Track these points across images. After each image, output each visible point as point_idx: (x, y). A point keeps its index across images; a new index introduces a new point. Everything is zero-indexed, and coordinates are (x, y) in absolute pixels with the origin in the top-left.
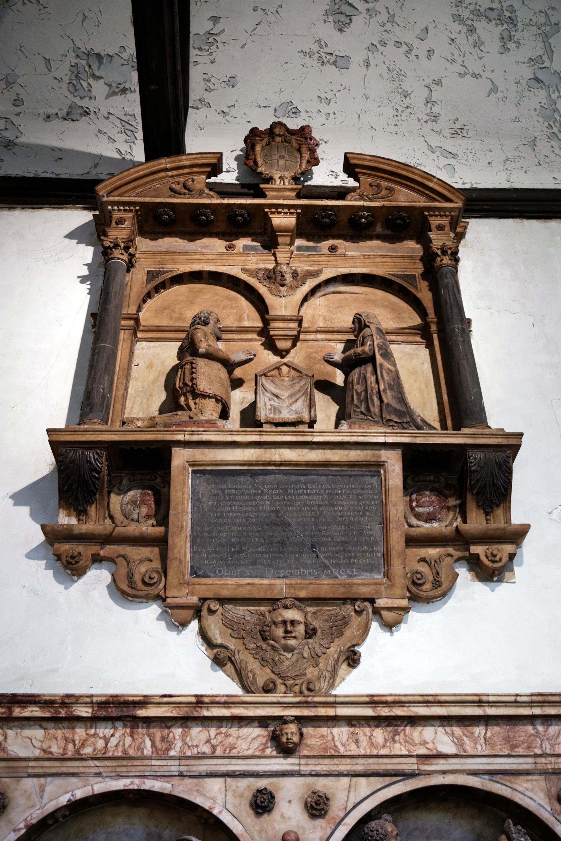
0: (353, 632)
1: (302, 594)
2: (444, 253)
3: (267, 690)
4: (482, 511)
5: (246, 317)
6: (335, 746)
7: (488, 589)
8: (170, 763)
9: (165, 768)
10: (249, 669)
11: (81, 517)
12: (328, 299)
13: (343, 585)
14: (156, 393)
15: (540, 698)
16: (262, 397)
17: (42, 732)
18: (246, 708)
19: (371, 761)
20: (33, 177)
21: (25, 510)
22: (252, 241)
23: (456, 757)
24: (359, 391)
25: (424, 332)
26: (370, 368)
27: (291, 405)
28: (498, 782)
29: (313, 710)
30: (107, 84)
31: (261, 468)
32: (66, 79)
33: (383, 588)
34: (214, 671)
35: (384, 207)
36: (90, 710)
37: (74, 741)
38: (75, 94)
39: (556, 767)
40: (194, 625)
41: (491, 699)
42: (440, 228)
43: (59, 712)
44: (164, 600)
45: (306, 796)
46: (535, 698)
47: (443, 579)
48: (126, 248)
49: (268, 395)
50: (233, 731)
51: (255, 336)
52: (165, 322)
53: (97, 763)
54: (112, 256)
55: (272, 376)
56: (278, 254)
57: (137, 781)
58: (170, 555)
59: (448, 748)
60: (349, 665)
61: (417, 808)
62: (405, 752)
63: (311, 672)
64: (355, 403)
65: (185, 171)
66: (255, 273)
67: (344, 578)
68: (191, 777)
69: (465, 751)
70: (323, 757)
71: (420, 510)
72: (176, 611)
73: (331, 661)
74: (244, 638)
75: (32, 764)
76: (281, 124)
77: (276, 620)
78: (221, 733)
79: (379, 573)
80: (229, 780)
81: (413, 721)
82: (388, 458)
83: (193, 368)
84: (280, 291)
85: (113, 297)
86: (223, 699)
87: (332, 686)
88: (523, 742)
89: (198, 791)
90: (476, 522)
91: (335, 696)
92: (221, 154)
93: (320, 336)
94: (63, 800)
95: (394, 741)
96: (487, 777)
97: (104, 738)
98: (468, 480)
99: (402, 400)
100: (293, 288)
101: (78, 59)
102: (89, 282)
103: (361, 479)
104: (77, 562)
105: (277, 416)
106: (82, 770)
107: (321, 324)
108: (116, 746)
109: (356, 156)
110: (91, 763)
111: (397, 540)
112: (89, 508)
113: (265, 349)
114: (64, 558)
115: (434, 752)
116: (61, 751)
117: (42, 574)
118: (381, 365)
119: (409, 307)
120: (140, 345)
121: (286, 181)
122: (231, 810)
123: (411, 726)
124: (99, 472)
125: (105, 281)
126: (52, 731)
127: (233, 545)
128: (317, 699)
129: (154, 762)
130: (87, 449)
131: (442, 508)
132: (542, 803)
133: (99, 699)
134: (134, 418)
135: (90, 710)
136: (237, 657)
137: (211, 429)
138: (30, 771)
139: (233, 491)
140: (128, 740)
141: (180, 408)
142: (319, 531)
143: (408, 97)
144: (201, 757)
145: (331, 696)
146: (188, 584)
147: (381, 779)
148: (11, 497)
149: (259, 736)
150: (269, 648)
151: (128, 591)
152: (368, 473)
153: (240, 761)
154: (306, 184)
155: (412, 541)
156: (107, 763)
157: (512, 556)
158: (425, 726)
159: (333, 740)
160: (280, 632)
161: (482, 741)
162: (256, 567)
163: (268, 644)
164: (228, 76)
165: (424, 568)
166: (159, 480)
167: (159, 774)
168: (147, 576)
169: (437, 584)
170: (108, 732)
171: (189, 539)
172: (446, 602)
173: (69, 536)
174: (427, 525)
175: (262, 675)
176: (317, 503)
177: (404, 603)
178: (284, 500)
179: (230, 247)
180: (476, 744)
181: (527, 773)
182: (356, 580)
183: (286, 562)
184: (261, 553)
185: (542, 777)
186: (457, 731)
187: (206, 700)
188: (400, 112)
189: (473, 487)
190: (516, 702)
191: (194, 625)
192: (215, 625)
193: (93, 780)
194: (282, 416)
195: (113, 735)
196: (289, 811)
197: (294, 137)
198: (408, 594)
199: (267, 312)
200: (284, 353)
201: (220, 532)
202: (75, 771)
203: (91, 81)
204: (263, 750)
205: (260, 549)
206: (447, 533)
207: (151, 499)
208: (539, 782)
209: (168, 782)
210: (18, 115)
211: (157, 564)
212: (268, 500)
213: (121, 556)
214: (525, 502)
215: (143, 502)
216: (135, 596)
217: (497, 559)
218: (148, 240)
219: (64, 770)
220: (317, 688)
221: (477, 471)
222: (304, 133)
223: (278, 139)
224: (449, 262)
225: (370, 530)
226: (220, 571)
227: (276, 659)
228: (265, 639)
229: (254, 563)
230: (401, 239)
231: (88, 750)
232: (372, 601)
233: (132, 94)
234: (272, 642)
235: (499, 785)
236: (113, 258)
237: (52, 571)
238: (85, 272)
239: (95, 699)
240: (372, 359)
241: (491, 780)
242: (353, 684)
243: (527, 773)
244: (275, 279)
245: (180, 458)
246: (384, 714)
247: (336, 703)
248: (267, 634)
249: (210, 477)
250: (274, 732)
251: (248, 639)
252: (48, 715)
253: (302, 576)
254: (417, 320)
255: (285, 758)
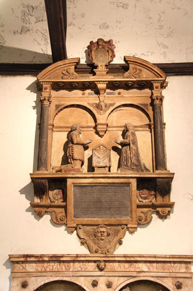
0: (121, 235)
1: (106, 223)
2: (157, 99)
3: (96, 252)
4: (161, 197)
5: (89, 122)
6: (114, 268)
7: (162, 221)
8: (70, 273)
9: (69, 274)
10: (91, 245)
11: (41, 199)
12: (120, 114)
13: (118, 220)
14: (60, 152)
15: (172, 256)
16: (94, 158)
17: (35, 264)
18: (90, 258)
19: (124, 273)
20: (13, 64)
21: (24, 196)
22: (91, 90)
23: (148, 272)
24: (125, 156)
25: (149, 126)
26: (128, 148)
27: (103, 161)
28: (159, 279)
29: (108, 258)
30: (36, 18)
31: (94, 184)
32: (20, 17)
33: (130, 221)
34: (81, 246)
35: (137, 80)
36: (48, 259)
37: (44, 267)
38: (24, 22)
39: (176, 276)
40: (75, 232)
41: (158, 256)
42: (157, 87)
43: (40, 259)
44: (66, 225)
45: (106, 282)
46: (171, 256)
47: (148, 218)
48: (48, 100)
49: (96, 157)
50: (87, 264)
51: (92, 129)
52: (62, 125)
53: (51, 273)
54: (44, 104)
55: (97, 150)
56: (100, 97)
57: (61, 278)
58: (68, 212)
59: (146, 269)
60: (119, 244)
61: (137, 285)
62: (133, 270)
63: (108, 247)
64: (123, 161)
65: (67, 65)
66: (92, 105)
67: (118, 218)
68: (76, 276)
69: (150, 270)
70: (111, 271)
71: (142, 196)
72: (70, 228)
73: (114, 243)
74: (89, 236)
75: (33, 273)
76: (101, 40)
77: (98, 231)
78: (83, 265)
79: (129, 216)
80: (86, 277)
81: (136, 262)
82: (132, 181)
83: (72, 149)
84: (100, 113)
85: (45, 120)
86: (84, 255)
87: (114, 250)
88: (167, 268)
89: (77, 280)
90: (160, 200)
91: (115, 255)
92: (80, 58)
93: (114, 129)
94: (43, 283)
95: (131, 267)
96: (156, 278)
97: (52, 266)
98: (157, 188)
99: (138, 160)
100: (105, 111)
101: (24, 8)
102: (36, 109)
103: (124, 187)
104: (41, 214)
105: (99, 165)
106: (47, 275)
107: (115, 125)
108: (55, 268)
109: (128, 57)
110: (49, 273)
111: (134, 206)
112: (43, 196)
113: (96, 134)
114: (37, 212)
115: (142, 271)
116: (41, 269)
117: (30, 216)
118: (132, 147)
119: (145, 115)
120: (54, 133)
121: (103, 67)
122: (87, 286)
123: (136, 263)
124: (46, 186)
125: (41, 108)
126: (38, 264)
127: (86, 208)
128: (109, 256)
129: (66, 273)
130: (42, 179)
131: (149, 195)
132: (171, 286)
133: (50, 256)
134: (55, 167)
135: (48, 259)
136: (87, 242)
137: (79, 173)
138: (33, 275)
139: (86, 192)
140: (59, 266)
141: (69, 163)
142: (111, 204)
143: (151, 19)
144: (78, 271)
145: (113, 255)
146: (73, 220)
147: (127, 278)
148: (19, 191)
149: (94, 265)
150: (97, 239)
151: (56, 222)
152: (126, 186)
153: (89, 272)
154: (111, 63)
155: (139, 206)
156: (53, 273)
157: (169, 212)
158: (139, 263)
159: (114, 267)
160: (99, 235)
161: (155, 268)
162: (93, 215)
163: (96, 238)
164: (82, 13)
165: (142, 215)
166: (63, 186)
167: (67, 276)
168: (61, 218)
169: (146, 220)
170: (53, 264)
171: (73, 206)
172: (149, 225)
173: (38, 206)
174: (144, 201)
175: (95, 247)
176: (111, 195)
177: (136, 226)
178: (101, 194)
179: (83, 94)
180: (153, 268)
181: (167, 277)
182: (122, 219)
183: (101, 213)
184: (94, 210)
185: (172, 278)
186: (148, 264)
187: (79, 256)
188: (148, 26)
189: (158, 190)
190: (165, 257)
191: (75, 232)
192: (81, 232)
193: (50, 278)
194: (100, 164)
195: (54, 265)
196: (102, 282)
197: (106, 44)
198: (137, 223)
199: (97, 122)
200: (102, 136)
201: (82, 204)
202: (45, 275)
203: (29, 16)
204: (95, 269)
205: (94, 209)
206: (150, 204)
207: (61, 192)
208: (170, 280)
209: (70, 278)
210: (3, 31)
211: (64, 214)
212: (96, 194)
213: (53, 211)
214: (174, 197)
215: (59, 194)
216: (58, 224)
217: (164, 213)
218: (55, 91)
219: (42, 275)
220: (110, 251)
221: (160, 185)
222: (110, 42)
223: (100, 47)
224: (159, 103)
225: (126, 203)
226: (82, 216)
227: (99, 242)
228: (95, 237)
229: (92, 213)
230: (144, 89)
231: (48, 269)
232: (127, 225)
233: (45, 21)
234: (97, 238)
235: (159, 280)
236: (44, 105)
237: (33, 216)
238: (34, 105)
239: (49, 256)
240: (129, 145)
241: (157, 279)
242: (120, 251)
243: (167, 277)
244: (99, 108)
245: (69, 182)
246: (128, 260)
247: (115, 257)
248: (96, 235)
249: (78, 187)
250: (98, 264)
251: (91, 236)
252: (37, 260)
253: (106, 217)
254: (148, 122)
255: (101, 271)
